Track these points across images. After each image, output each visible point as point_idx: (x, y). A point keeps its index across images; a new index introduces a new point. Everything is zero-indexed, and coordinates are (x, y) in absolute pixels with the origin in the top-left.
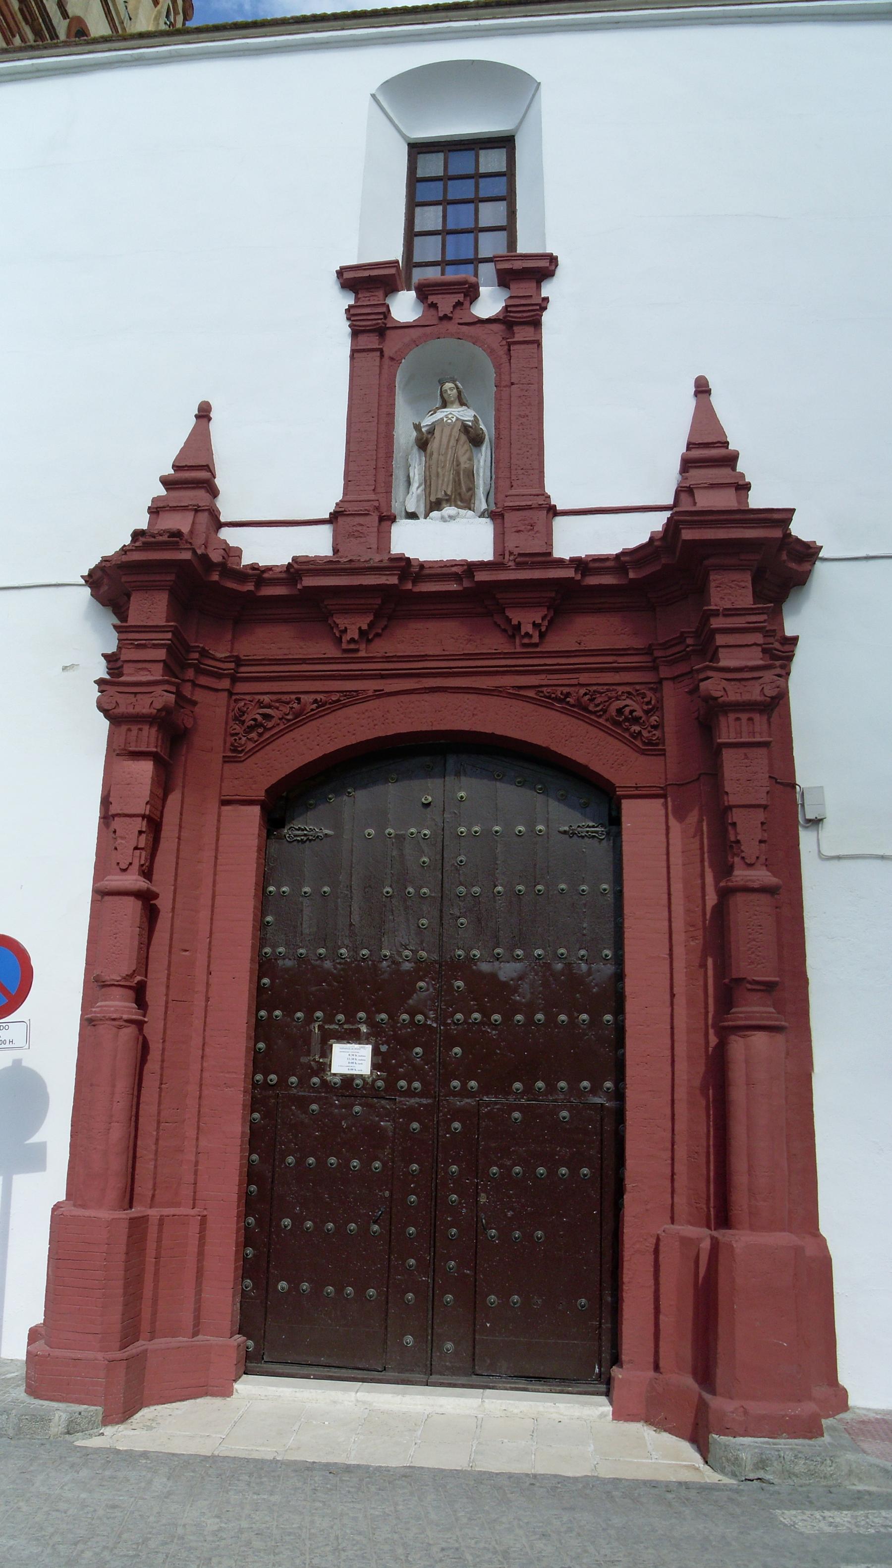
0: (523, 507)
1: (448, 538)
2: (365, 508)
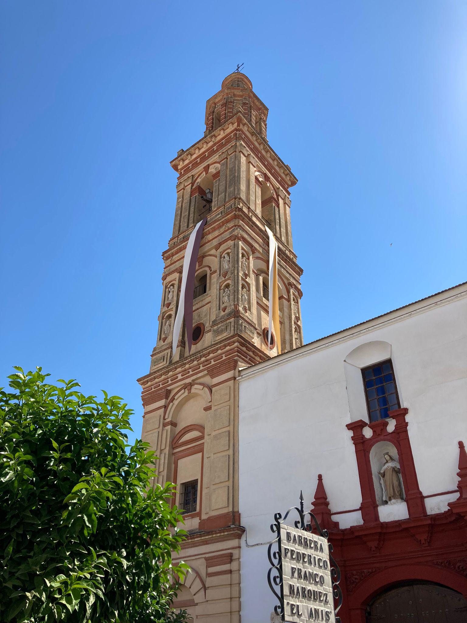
0: (414, 497)
1: (394, 511)
2: (369, 506)
